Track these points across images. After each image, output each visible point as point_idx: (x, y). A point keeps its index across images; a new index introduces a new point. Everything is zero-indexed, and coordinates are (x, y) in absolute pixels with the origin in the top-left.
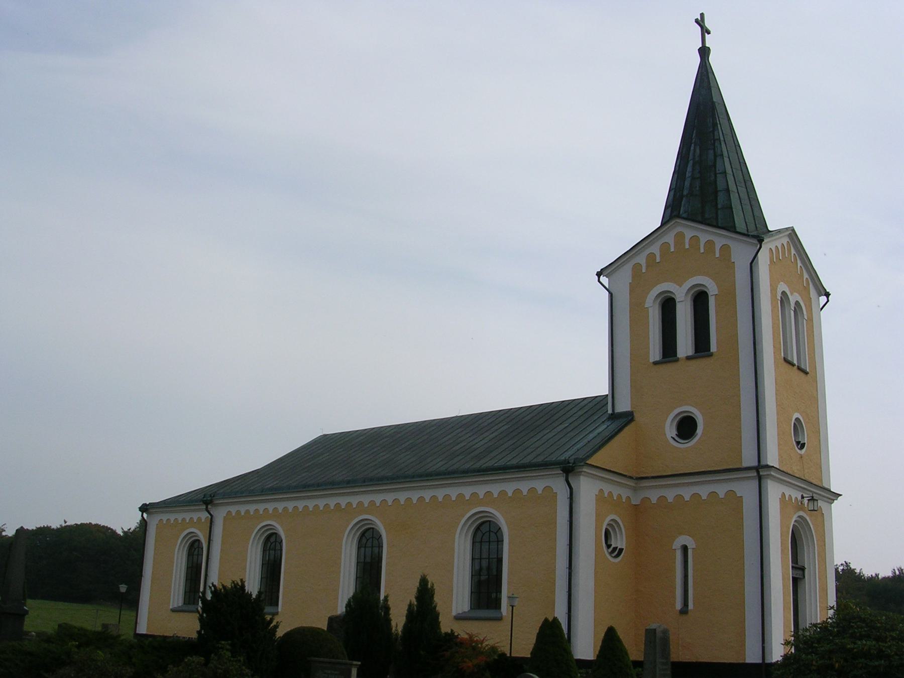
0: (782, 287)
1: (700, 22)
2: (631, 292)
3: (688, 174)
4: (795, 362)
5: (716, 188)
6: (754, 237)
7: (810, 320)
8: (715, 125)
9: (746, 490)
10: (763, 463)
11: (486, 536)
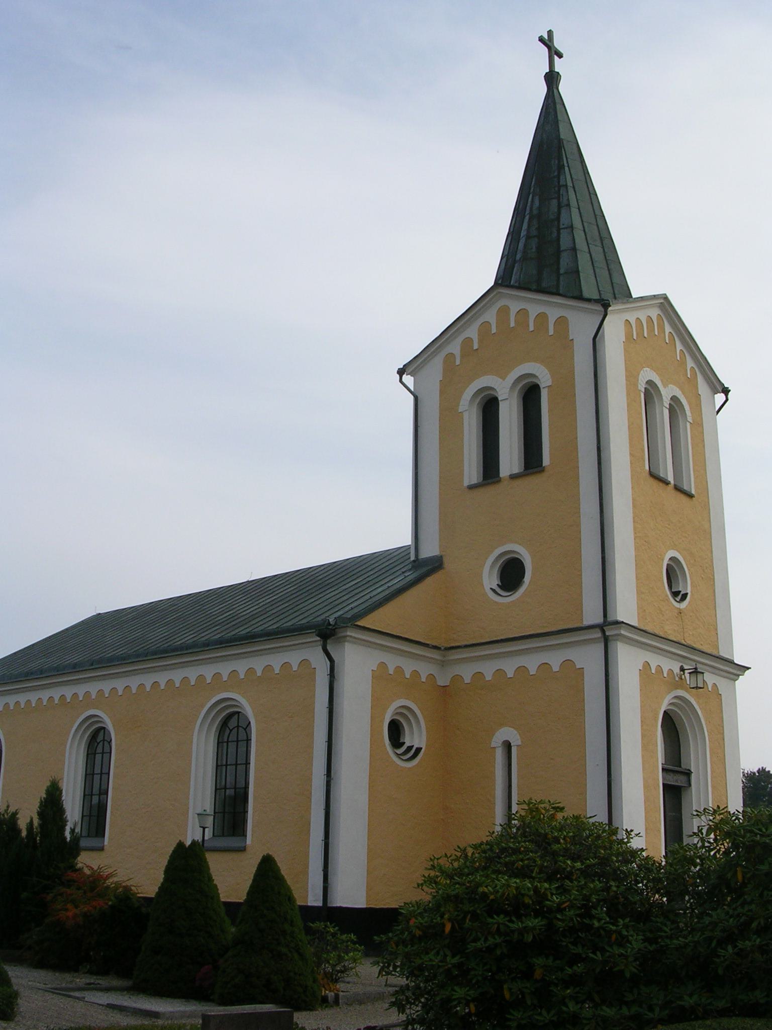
0: (647, 374)
1: (547, 42)
2: (442, 392)
3: (523, 233)
4: (671, 478)
5: (559, 245)
6: (596, 301)
7: (698, 425)
8: (561, 168)
9: (588, 658)
10: (610, 618)
11: (232, 730)
